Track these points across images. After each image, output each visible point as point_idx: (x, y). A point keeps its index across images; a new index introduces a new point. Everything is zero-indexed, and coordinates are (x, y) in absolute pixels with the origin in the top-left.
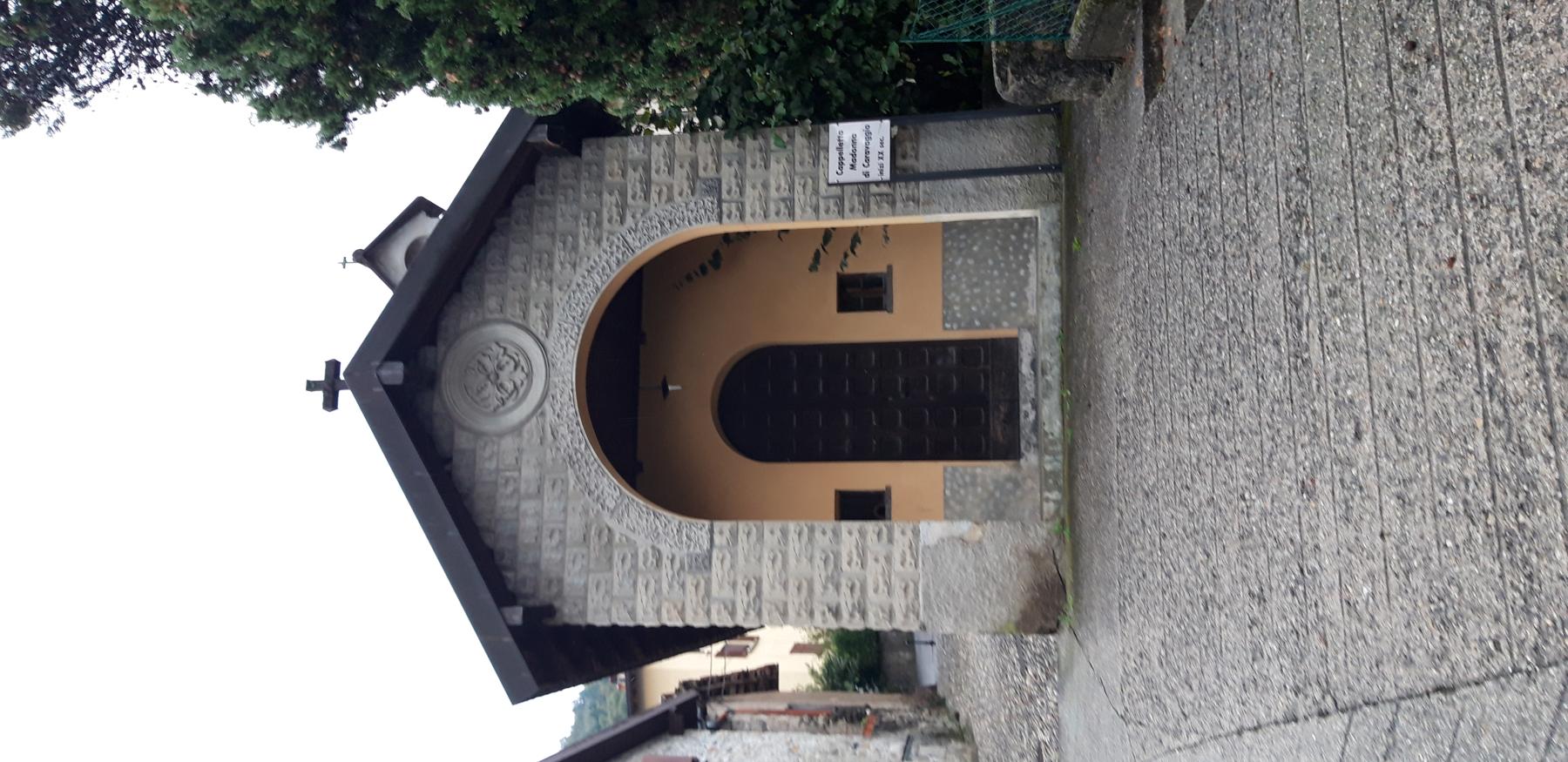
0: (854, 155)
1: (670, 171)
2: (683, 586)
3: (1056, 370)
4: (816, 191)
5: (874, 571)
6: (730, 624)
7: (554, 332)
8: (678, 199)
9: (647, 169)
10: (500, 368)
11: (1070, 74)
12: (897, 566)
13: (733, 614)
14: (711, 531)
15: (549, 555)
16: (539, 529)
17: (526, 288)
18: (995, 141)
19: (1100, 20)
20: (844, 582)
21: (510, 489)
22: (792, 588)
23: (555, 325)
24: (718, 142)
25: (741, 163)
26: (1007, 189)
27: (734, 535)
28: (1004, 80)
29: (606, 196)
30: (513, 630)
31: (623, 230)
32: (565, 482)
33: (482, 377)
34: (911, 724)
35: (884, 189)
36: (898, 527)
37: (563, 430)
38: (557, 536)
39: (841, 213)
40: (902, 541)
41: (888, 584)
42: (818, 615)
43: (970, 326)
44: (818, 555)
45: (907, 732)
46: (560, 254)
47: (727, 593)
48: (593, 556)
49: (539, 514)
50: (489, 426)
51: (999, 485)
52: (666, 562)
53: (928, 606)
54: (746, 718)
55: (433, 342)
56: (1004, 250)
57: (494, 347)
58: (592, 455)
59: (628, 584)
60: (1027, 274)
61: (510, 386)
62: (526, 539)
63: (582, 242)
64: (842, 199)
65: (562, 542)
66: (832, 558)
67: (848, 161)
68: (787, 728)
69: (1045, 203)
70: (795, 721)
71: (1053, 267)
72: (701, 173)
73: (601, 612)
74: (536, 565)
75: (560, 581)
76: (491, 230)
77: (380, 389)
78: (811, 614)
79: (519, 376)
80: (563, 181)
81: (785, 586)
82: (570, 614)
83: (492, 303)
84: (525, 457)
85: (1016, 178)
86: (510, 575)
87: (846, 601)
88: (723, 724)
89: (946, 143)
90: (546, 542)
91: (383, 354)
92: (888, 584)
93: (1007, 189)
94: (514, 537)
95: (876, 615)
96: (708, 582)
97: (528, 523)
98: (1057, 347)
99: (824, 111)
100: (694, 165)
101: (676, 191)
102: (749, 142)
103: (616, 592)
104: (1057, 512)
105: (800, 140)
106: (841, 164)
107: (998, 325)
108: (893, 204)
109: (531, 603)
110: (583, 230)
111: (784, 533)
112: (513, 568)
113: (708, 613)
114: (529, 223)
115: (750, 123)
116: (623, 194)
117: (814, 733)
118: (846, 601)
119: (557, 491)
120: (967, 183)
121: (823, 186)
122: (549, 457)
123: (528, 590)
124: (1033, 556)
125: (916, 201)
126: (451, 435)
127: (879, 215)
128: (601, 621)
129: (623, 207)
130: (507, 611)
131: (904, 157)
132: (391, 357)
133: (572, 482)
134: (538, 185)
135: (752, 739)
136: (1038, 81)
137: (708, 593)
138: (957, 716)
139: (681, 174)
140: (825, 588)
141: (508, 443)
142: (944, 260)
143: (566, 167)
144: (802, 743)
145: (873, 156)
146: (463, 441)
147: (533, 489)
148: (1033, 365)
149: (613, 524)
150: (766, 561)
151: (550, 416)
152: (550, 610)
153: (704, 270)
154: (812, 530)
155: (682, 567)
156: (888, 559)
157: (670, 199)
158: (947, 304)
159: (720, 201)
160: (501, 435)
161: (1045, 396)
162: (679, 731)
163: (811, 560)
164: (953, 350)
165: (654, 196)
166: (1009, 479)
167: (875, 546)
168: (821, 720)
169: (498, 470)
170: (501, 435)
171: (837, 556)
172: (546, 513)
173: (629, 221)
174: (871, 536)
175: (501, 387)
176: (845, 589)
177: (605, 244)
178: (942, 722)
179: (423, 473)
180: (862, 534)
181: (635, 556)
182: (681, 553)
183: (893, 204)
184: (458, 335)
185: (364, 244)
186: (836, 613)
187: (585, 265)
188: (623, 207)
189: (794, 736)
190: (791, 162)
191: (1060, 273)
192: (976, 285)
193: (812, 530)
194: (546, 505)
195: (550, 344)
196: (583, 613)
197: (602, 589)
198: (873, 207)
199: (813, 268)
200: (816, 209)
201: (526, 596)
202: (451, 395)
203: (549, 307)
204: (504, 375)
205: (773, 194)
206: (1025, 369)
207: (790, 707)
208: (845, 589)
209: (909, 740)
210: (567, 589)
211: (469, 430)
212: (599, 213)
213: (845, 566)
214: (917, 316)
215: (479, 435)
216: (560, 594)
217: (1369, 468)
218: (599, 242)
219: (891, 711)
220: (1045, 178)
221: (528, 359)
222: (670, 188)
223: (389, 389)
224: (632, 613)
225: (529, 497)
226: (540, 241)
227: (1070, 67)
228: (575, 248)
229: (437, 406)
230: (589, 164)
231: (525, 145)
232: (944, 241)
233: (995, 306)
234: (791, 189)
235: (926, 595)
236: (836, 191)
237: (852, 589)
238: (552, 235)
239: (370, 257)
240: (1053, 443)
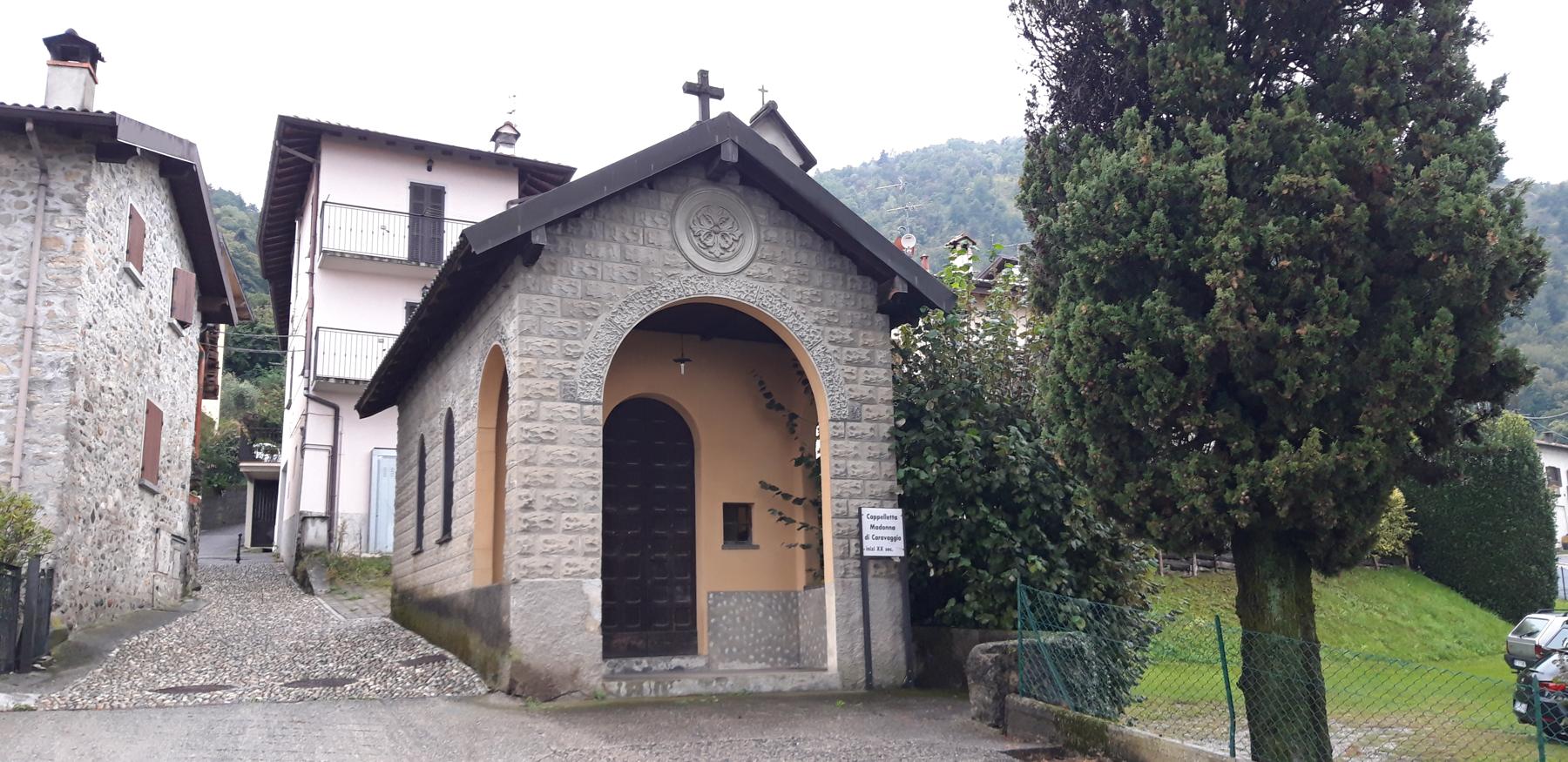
0: (881, 528)
1: (867, 383)
2: (550, 377)
3: (721, 690)
4: (851, 497)
5: (562, 540)
7: (750, 282)
8: (847, 387)
9: (868, 364)
11: (995, 698)
12: (566, 560)
14: (595, 403)
15: (576, 265)
17: (784, 262)
18: (889, 642)
19: (1040, 719)
20: (553, 514)
21: (629, 236)
22: (548, 470)
23: (756, 283)
24: (887, 421)
25: (872, 439)
26: (853, 646)
28: (989, 651)
29: (849, 331)
30: (528, 235)
31: (825, 343)
32: (635, 282)
33: (717, 220)
35: (853, 551)
37: (676, 283)
38: (592, 272)
39: (836, 516)
42: (525, 492)
43: (710, 615)
44: (575, 493)
46: (808, 291)
47: (544, 415)
48: (576, 302)
49: (609, 259)
52: (570, 364)
53: (534, 586)
55: (743, 182)
56: (770, 642)
57: (739, 233)
60: (750, 662)
61: (709, 242)
63: (816, 309)
64: (847, 517)
66: (571, 505)
67: (877, 523)
71: (796, 685)
72: (865, 407)
74: (567, 253)
75: (554, 273)
76: (826, 238)
78: (526, 486)
79: (717, 251)
80: (860, 297)
81: (549, 464)
83: (773, 234)
85: (861, 654)
87: (537, 516)
89: (887, 600)
90: (587, 263)
91: (744, 147)
93: (853, 646)
95: (526, 542)
96: (553, 399)
98: (737, 690)
99: (911, 502)
100: (871, 401)
101: (853, 386)
102: (887, 445)
104: (611, 693)
106: (874, 518)
108: (842, 558)
110: (825, 311)
114: (830, 269)
115: (902, 446)
116: (852, 344)
118: (537, 516)
119: (628, 276)
120: (859, 613)
121: (856, 502)
122: (655, 271)
126: (671, 191)
127: (834, 546)
129: (839, 343)
131: (876, 566)
132: (742, 153)
134: (857, 278)
136: (990, 674)
137: (543, 398)
139: (864, 390)
140: (549, 498)
142: (763, 593)
143: (871, 301)
146: (667, 200)
147: (629, 255)
148: (679, 669)
149: (601, 320)
150: (570, 449)
151: (686, 274)
153: (768, 395)
155: (565, 377)
156: (572, 552)
157: (847, 381)
158: (728, 595)
159: (845, 421)
160: (672, 232)
161: (701, 681)
164: (688, 599)
165: (849, 369)
167: (583, 541)
169: (645, 227)
170: (672, 232)
171: (574, 509)
172: (609, 265)
173: (831, 348)
174: (590, 538)
176: (547, 515)
177: (815, 327)
180: (592, 531)
181: (575, 337)
182: (577, 377)
183: (842, 558)
184: (748, 204)
185: (780, 110)
186: (527, 508)
187: (800, 311)
188: (839, 343)
190: (873, 478)
191: (792, 691)
192: (743, 619)
194: (616, 266)
195: (741, 277)
197: (548, 309)
198: (841, 542)
199: (764, 485)
200: (839, 497)
202: (702, 194)
203: (770, 279)
205: (851, 463)
206: (676, 661)
208: (547, 515)
210: (548, 278)
211: (676, 207)
212: (837, 324)
213: (565, 516)
214: (718, 570)
216: (544, 271)
218: (817, 323)
220: (861, 678)
221: (729, 259)
222: (854, 382)
223: (716, 150)
225: (623, 251)
226: (817, 276)
227: (1000, 698)
228: (812, 303)
229: (694, 181)
230: (872, 319)
231: (894, 274)
232: (777, 593)
233: (726, 636)
234: (854, 477)
235: (542, 584)
236: (855, 512)
237: (547, 521)
238: (821, 287)
239: (770, 114)
240: (665, 688)
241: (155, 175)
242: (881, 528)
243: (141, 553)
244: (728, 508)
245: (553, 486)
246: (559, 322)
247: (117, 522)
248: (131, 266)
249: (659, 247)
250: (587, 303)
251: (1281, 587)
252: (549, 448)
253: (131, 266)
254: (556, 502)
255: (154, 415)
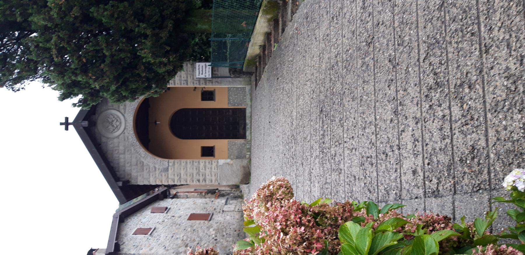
0: (202, 71)
2: (162, 175)
5: (208, 171)
6: (173, 184)
7: (127, 112)
10: (113, 121)
11: (244, 75)
12: (213, 170)
13: (174, 182)
14: (168, 162)
15: (128, 168)
16: (125, 162)
21: (116, 152)
22: (188, 175)
23: (127, 111)
27: (174, 163)
30: (120, 187)
32: (131, 150)
34: (228, 194)
36: (214, 160)
37: (130, 137)
40: (214, 164)
41: (211, 174)
43: (234, 105)
45: (227, 197)
47: (172, 177)
49: (124, 158)
50: (111, 136)
51: (241, 145)
52: (157, 170)
54: (182, 194)
58: (138, 143)
59: (148, 175)
62: (121, 164)
65: (131, 165)
66: (198, 169)
67: (201, 72)
68: (194, 197)
69: (248, 85)
70: (196, 194)
73: (141, 182)
74: (124, 171)
75: (131, 174)
77: (82, 128)
79: (118, 123)
81: (187, 175)
82: (133, 182)
84: (120, 144)
86: (117, 173)
87: (201, 178)
88: (175, 196)
90: (127, 165)
92: (211, 174)
94: (118, 164)
96: (168, 174)
97: (122, 160)
103: (145, 177)
105: (189, 65)
106: (199, 73)
107: (241, 105)
108: (212, 83)
109: (123, 180)
111: (186, 163)
112: (118, 171)
113: (168, 181)
117: (201, 198)
118: (201, 178)
123: (122, 176)
124: (244, 167)
125: (218, 82)
128: (141, 183)
130: (118, 183)
132: (84, 120)
133: (133, 150)
135: (183, 201)
137: (168, 177)
138: (241, 191)
141: (116, 140)
142: (229, 93)
144: (197, 201)
145: (207, 72)
146: (104, 140)
147: (123, 152)
149: (143, 160)
151: (126, 134)
152: (128, 181)
154: (193, 162)
156: (211, 168)
158: (229, 100)
160: (114, 138)
162: (162, 199)
163: (193, 169)
164: (250, 28)
166: (243, 144)
168: (203, 194)
170: (114, 138)
171: (199, 168)
175: (113, 126)
176: (201, 175)
178: (237, 193)
179: (94, 149)
181: (149, 168)
182: (161, 168)
183: (212, 83)
184: (101, 112)
186: (199, 181)
189: (195, 199)
193: (193, 162)
195: (126, 115)
196: (137, 182)
200: (193, 83)
201: (122, 178)
202: (100, 128)
204: (114, 123)
205: (183, 79)
207: (195, 190)
208: (201, 175)
209: (227, 199)
213: (201, 170)
214: (221, 102)
215: (108, 138)
217: (372, 112)
219: (223, 191)
221: (120, 119)
223: (84, 128)
224: (149, 182)
225: (121, 154)
233: (241, 101)
234: (187, 78)
241: (124, 224)
242: (202, 71)
243: (228, 218)
244: (203, 99)
245: (193, 174)
246: (145, 172)
247: (218, 229)
248: (149, 233)
249: (119, 142)
250: (139, 165)
251: (197, 25)
252: (182, 175)
253: (149, 233)
254: (197, 173)
255: (193, 217)
